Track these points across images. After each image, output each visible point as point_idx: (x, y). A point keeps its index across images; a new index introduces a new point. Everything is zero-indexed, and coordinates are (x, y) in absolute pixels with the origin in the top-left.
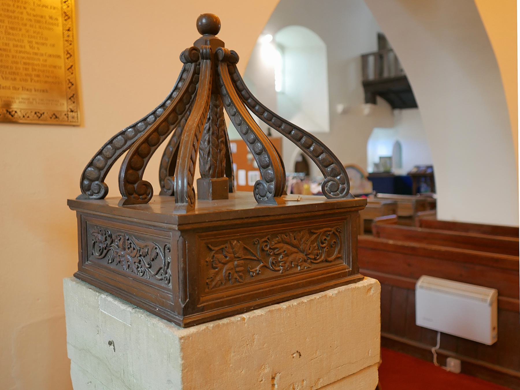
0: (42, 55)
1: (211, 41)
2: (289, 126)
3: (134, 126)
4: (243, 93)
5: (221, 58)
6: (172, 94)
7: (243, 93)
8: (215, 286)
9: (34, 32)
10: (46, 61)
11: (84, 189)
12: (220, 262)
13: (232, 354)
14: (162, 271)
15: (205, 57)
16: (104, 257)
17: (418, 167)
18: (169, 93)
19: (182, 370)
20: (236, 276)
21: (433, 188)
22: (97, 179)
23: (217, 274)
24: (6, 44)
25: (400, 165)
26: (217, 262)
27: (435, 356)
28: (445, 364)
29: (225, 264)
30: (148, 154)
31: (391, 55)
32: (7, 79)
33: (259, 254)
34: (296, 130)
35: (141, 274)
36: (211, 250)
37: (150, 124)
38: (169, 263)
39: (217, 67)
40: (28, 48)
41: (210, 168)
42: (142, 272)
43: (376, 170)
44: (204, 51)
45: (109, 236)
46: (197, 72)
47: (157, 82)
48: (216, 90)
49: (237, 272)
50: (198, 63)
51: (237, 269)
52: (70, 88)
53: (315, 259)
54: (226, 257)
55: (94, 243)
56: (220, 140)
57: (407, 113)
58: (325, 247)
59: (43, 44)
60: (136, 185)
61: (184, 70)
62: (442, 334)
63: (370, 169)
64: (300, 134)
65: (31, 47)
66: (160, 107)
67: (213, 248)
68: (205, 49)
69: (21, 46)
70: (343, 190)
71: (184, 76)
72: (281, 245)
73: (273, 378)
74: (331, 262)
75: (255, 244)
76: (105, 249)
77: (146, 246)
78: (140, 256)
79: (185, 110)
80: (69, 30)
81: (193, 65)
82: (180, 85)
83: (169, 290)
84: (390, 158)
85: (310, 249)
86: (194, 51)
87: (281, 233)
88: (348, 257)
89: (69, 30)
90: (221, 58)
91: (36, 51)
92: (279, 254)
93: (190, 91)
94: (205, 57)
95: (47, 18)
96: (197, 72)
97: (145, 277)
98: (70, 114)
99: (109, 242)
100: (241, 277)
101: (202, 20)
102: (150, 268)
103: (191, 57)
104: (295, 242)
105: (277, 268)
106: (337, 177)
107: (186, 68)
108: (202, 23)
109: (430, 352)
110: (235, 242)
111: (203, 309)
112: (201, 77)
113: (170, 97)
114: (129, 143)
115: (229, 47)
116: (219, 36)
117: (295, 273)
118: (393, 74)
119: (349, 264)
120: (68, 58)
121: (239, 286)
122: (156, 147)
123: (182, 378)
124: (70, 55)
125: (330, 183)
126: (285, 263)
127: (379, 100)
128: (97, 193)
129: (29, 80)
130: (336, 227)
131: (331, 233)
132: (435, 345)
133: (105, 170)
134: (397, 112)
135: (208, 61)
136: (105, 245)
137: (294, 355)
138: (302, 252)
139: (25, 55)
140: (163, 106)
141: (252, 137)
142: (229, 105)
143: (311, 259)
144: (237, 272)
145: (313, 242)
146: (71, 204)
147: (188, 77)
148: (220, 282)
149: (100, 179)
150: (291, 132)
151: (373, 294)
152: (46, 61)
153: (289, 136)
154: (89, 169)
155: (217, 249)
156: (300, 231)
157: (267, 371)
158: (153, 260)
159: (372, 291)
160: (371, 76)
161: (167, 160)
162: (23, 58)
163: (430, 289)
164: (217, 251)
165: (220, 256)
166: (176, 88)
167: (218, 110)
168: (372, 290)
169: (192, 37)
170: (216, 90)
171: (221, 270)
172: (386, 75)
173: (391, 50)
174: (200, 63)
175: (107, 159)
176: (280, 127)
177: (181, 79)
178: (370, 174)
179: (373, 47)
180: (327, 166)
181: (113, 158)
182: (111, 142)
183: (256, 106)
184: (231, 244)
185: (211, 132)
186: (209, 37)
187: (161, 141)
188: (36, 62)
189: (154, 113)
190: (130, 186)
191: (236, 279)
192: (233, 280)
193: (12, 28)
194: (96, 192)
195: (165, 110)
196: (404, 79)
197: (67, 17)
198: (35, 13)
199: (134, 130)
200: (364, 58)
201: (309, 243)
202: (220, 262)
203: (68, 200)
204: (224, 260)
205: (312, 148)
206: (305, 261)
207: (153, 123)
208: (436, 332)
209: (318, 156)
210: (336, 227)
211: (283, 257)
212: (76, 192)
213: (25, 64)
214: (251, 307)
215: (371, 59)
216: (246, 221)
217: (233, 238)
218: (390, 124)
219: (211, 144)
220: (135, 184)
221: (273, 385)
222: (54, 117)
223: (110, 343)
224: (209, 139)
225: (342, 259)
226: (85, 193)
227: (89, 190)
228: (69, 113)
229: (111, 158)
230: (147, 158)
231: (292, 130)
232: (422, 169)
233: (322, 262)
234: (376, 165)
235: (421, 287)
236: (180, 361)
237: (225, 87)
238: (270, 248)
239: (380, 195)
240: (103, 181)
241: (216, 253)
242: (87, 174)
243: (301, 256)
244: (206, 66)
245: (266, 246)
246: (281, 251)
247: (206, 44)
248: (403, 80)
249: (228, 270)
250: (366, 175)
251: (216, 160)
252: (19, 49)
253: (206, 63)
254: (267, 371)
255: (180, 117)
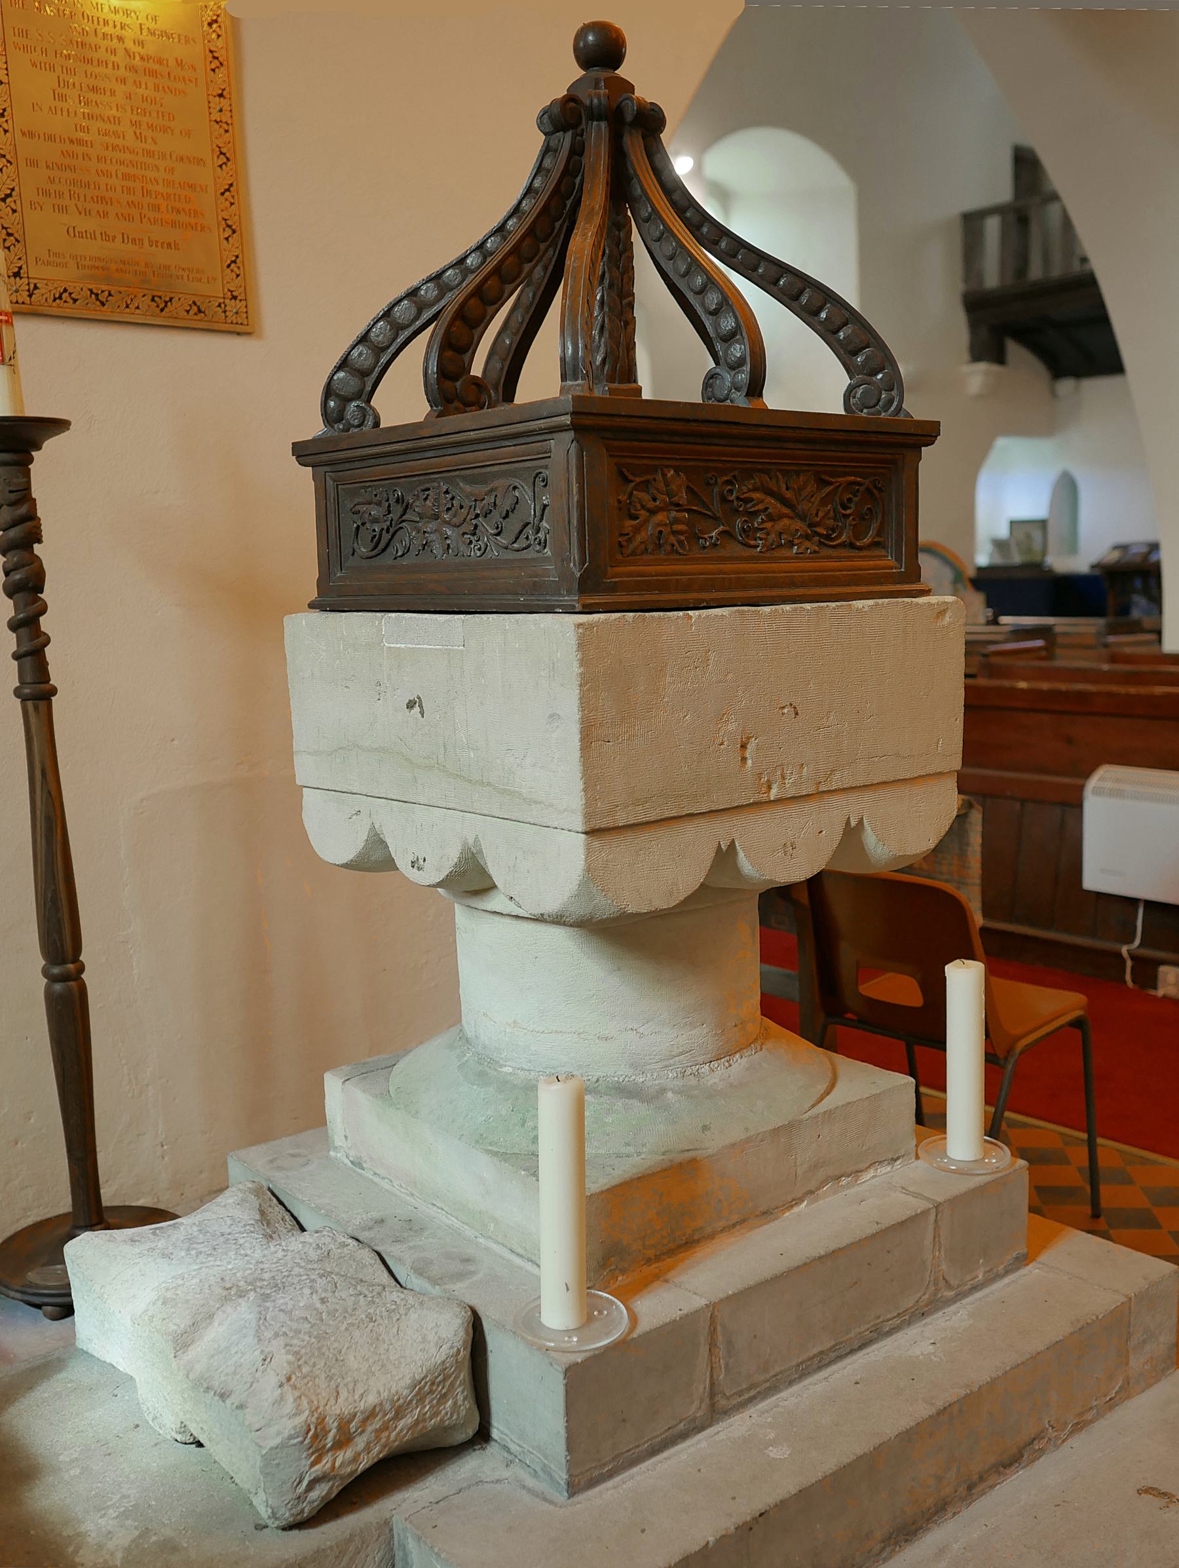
0: (163, 156)
1: (606, 80)
2: (774, 268)
3: (437, 278)
4: (676, 197)
5: (629, 118)
6: (520, 202)
7: (676, 197)
8: (633, 553)
9: (144, 99)
10: (172, 170)
11: (329, 417)
12: (643, 507)
13: (668, 679)
14: (529, 530)
15: (595, 115)
16: (384, 550)
17: (1124, 548)
18: (515, 202)
19: (581, 685)
20: (672, 539)
21: (1155, 598)
22: (358, 396)
23: (637, 529)
24: (82, 129)
25: (1072, 546)
26: (639, 506)
27: (1129, 964)
28: (1153, 983)
29: (652, 512)
30: (482, 321)
31: (1053, 210)
32: (88, 213)
33: (717, 508)
34: (789, 275)
35: (479, 553)
36: (627, 480)
37: (472, 272)
38: (545, 506)
39: (621, 137)
40: (130, 140)
41: (604, 361)
42: (479, 549)
43: (998, 560)
44: (595, 101)
45: (397, 501)
46: (577, 150)
47: (489, 176)
48: (621, 191)
49: (674, 533)
50: (579, 129)
51: (675, 527)
52: (227, 239)
53: (828, 537)
54: (655, 500)
55: (358, 527)
56: (624, 302)
57: (1096, 388)
58: (849, 515)
59: (164, 130)
60: (458, 384)
61: (547, 150)
62: (1150, 905)
63: (983, 558)
64: (799, 285)
65: (139, 137)
66: (494, 233)
67: (631, 477)
68: (597, 97)
69: (116, 134)
70: (891, 401)
71: (547, 163)
72: (757, 495)
73: (744, 746)
74: (860, 548)
75: (708, 484)
76: (388, 531)
77: (492, 490)
78: (477, 516)
79: (552, 231)
80: (221, 95)
81: (569, 135)
82: (537, 183)
83: (546, 560)
84: (1043, 524)
85: (817, 515)
86: (572, 104)
87: (760, 471)
88: (899, 547)
89: (221, 95)
90: (629, 118)
91: (149, 146)
92: (755, 514)
93: (563, 189)
94: (595, 115)
95: (172, 62)
96: (577, 150)
97: (488, 555)
98: (231, 305)
99: (397, 510)
100: (681, 543)
101: (586, 36)
102: (498, 534)
103: (564, 118)
104: (788, 495)
105: (753, 542)
106: (876, 374)
107: (551, 144)
108: (586, 41)
109: (1119, 955)
110: (672, 472)
111: (613, 589)
112: (587, 160)
113: (516, 210)
114: (426, 315)
115: (645, 92)
116: (621, 72)
117: (786, 558)
118: (1056, 272)
119: (899, 560)
120: (221, 166)
121: (678, 560)
122: (497, 306)
123: (580, 699)
124: (225, 157)
125: (860, 391)
126: (768, 534)
127: (1014, 349)
128: (359, 426)
129: (137, 217)
130: (872, 478)
131: (862, 488)
132: (1132, 941)
133: (375, 374)
134: (1066, 386)
135: (603, 124)
136: (388, 523)
137: (786, 711)
138: (803, 518)
139: (127, 156)
140: (501, 229)
141: (699, 281)
142: (647, 220)
143: (820, 535)
144: (674, 533)
145: (824, 502)
146: (303, 452)
147: (556, 165)
148: (643, 546)
149: (364, 397)
150: (778, 280)
151: (950, 623)
152: (172, 170)
153: (775, 289)
154: (341, 374)
155: (638, 480)
156: (798, 473)
157: (732, 727)
158: (507, 516)
159: (947, 619)
160: (992, 279)
161: (499, 366)
162: (122, 163)
163: (1119, 794)
164: (638, 484)
165: (645, 497)
166: (529, 191)
167: (622, 234)
168: (948, 615)
169: (563, 75)
170: (621, 191)
171: (646, 521)
172: (1036, 272)
173: (1055, 197)
174: (583, 131)
175: (379, 350)
176: (755, 269)
177: (539, 169)
178: (980, 570)
179: (1000, 188)
180: (855, 353)
181: (392, 349)
182: (387, 314)
183: (702, 226)
184: (664, 475)
185: (606, 282)
186: (600, 73)
187: (506, 295)
188: (151, 174)
189: (481, 246)
190: (448, 384)
191: (673, 545)
192: (669, 548)
193: (94, 89)
194: (356, 422)
195: (504, 238)
196: (1087, 284)
197: (215, 63)
198: (143, 52)
199: (439, 286)
200: (972, 221)
201: (816, 500)
202: (643, 507)
203: (295, 446)
204: (651, 505)
205: (823, 315)
206: (807, 537)
207: (479, 268)
208: (1133, 902)
209: (838, 331)
210: (872, 478)
211: (763, 521)
212: (313, 427)
213: (125, 177)
214: (703, 600)
215: (993, 226)
216: (694, 426)
217: (667, 463)
218: (1042, 424)
219: (606, 309)
220: (457, 380)
221: (744, 759)
222: (195, 309)
223: (411, 705)
224: (602, 296)
225: (884, 547)
226: (333, 427)
227: (340, 419)
228: (227, 301)
229: (388, 347)
230: (480, 329)
231: (782, 276)
232: (1134, 550)
233: (842, 545)
234: (1000, 545)
235: (1097, 792)
236: (576, 669)
237: (640, 182)
238: (738, 498)
239: (1004, 619)
240: (369, 400)
241: (635, 488)
242: (335, 385)
243: (798, 525)
244: (597, 135)
245: (731, 491)
246: (761, 507)
247: (597, 86)
248: (1085, 285)
249: (658, 525)
250: (971, 573)
251: (618, 344)
252: (111, 140)
253: (599, 127)
254: (732, 727)
255: (542, 246)
